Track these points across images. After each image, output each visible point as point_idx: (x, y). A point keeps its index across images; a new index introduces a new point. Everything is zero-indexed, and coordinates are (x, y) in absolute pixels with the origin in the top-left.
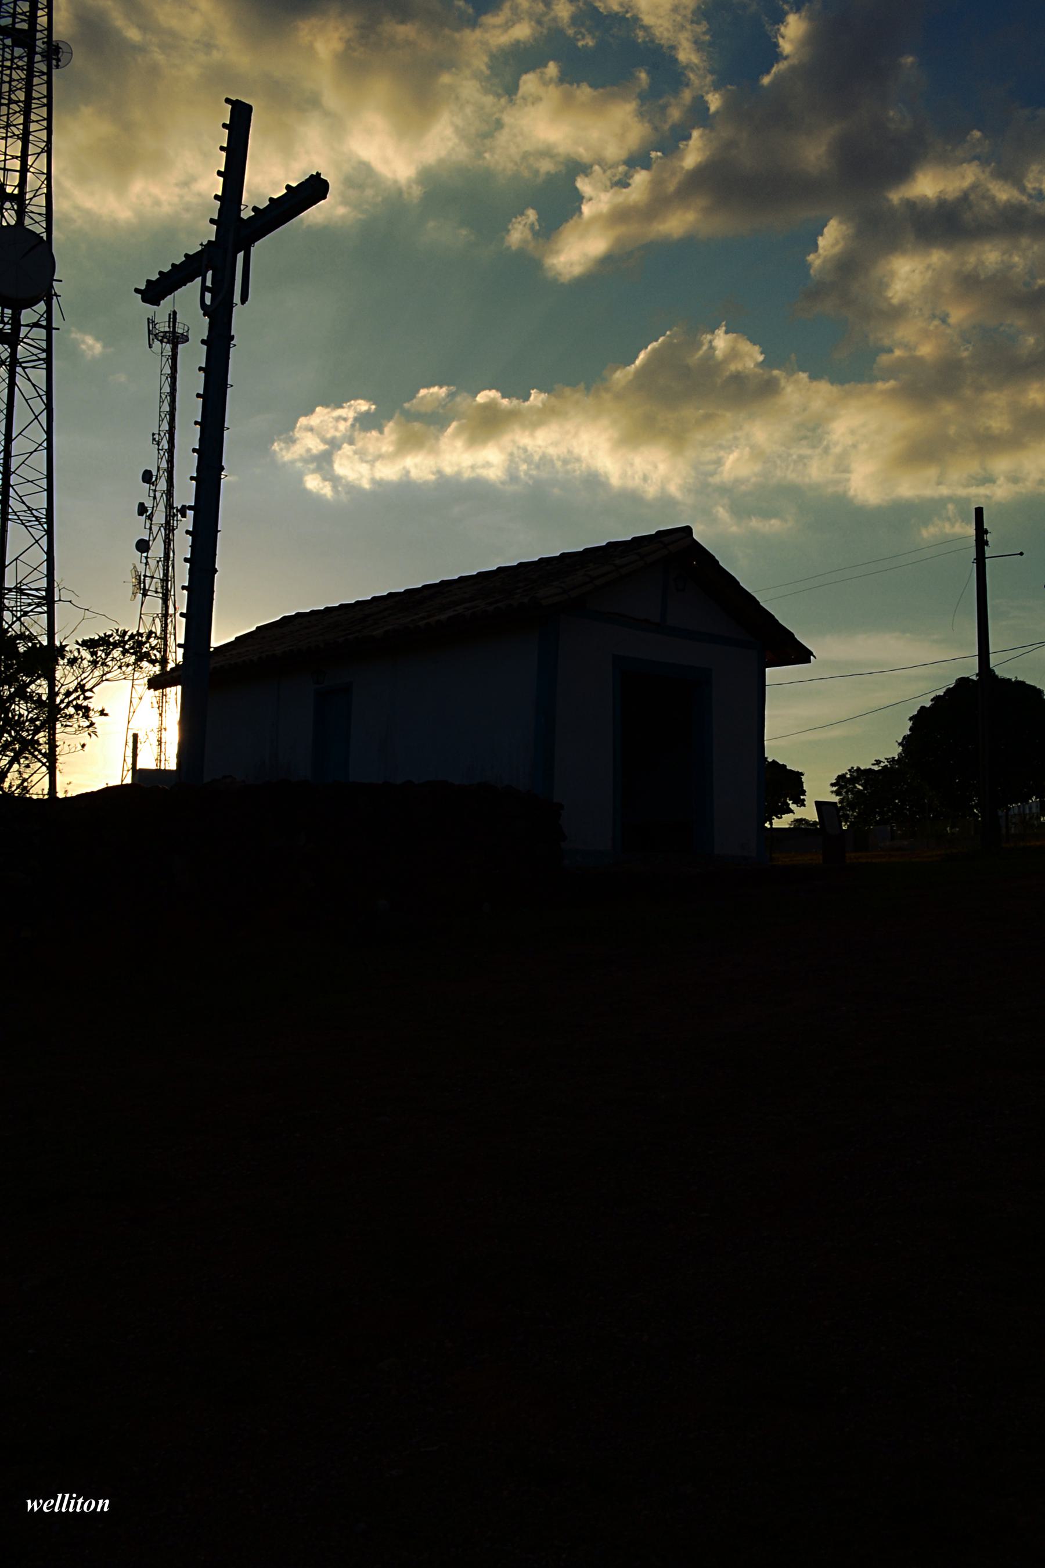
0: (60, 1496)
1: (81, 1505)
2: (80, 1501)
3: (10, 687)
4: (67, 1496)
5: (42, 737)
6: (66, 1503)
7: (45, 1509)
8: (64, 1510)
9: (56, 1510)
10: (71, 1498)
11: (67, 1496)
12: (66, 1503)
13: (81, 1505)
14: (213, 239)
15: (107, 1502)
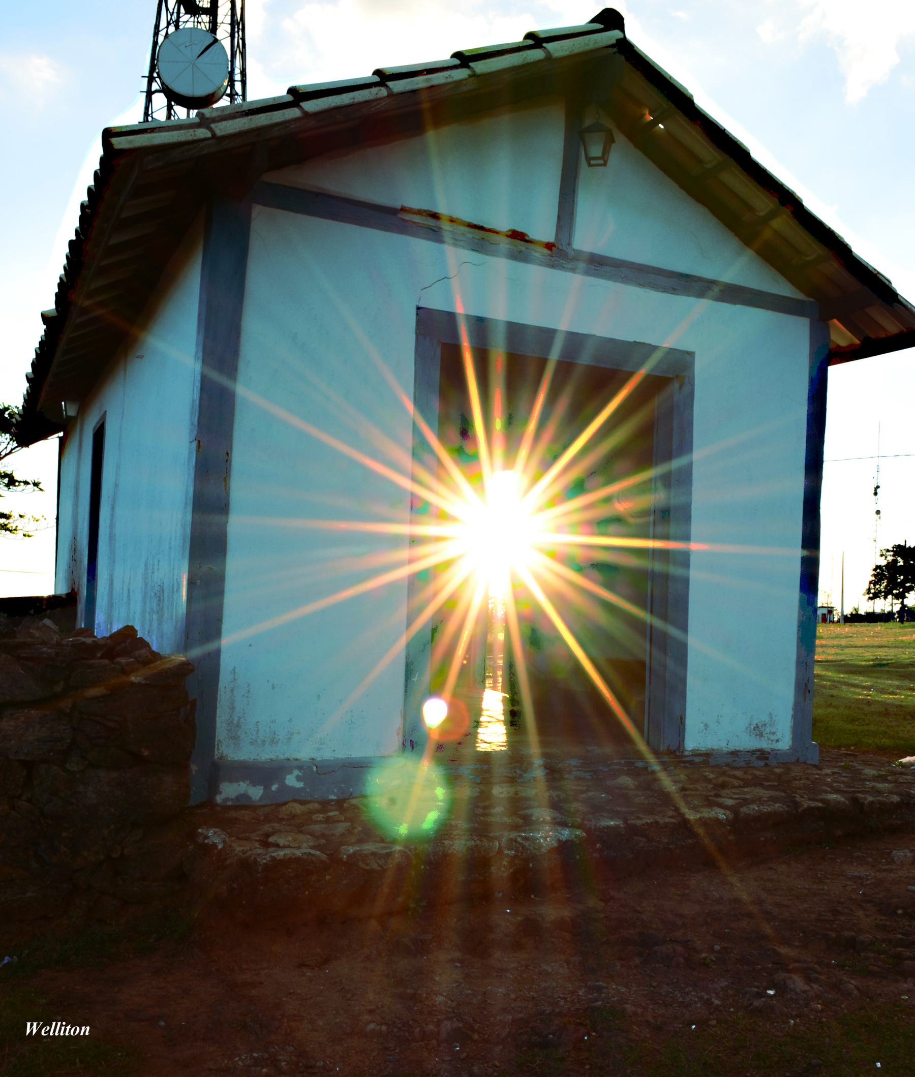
0: (54, 1023)
1: (69, 1031)
2: (69, 1027)
3: (240, 1056)
4: (59, 1023)
5: (59, 688)
6: (58, 1029)
7: (43, 1034)
8: (56, 1034)
9: (51, 1034)
10: (62, 1025)
11: (59, 1023)
12: (58, 1029)
13: (69, 1031)
14: (74, 238)
15: (88, 1028)
